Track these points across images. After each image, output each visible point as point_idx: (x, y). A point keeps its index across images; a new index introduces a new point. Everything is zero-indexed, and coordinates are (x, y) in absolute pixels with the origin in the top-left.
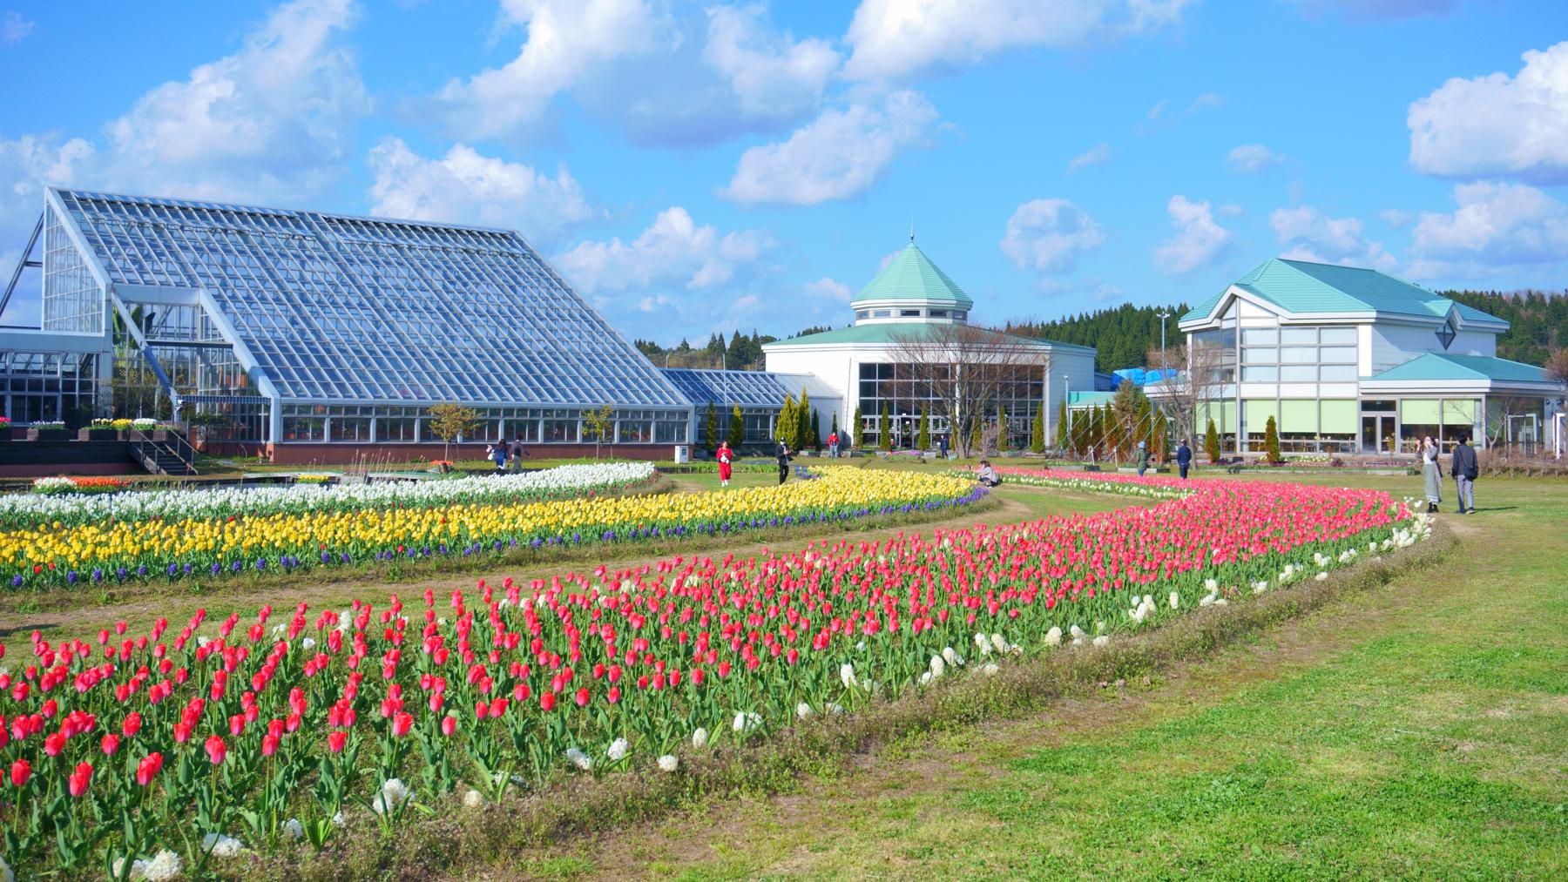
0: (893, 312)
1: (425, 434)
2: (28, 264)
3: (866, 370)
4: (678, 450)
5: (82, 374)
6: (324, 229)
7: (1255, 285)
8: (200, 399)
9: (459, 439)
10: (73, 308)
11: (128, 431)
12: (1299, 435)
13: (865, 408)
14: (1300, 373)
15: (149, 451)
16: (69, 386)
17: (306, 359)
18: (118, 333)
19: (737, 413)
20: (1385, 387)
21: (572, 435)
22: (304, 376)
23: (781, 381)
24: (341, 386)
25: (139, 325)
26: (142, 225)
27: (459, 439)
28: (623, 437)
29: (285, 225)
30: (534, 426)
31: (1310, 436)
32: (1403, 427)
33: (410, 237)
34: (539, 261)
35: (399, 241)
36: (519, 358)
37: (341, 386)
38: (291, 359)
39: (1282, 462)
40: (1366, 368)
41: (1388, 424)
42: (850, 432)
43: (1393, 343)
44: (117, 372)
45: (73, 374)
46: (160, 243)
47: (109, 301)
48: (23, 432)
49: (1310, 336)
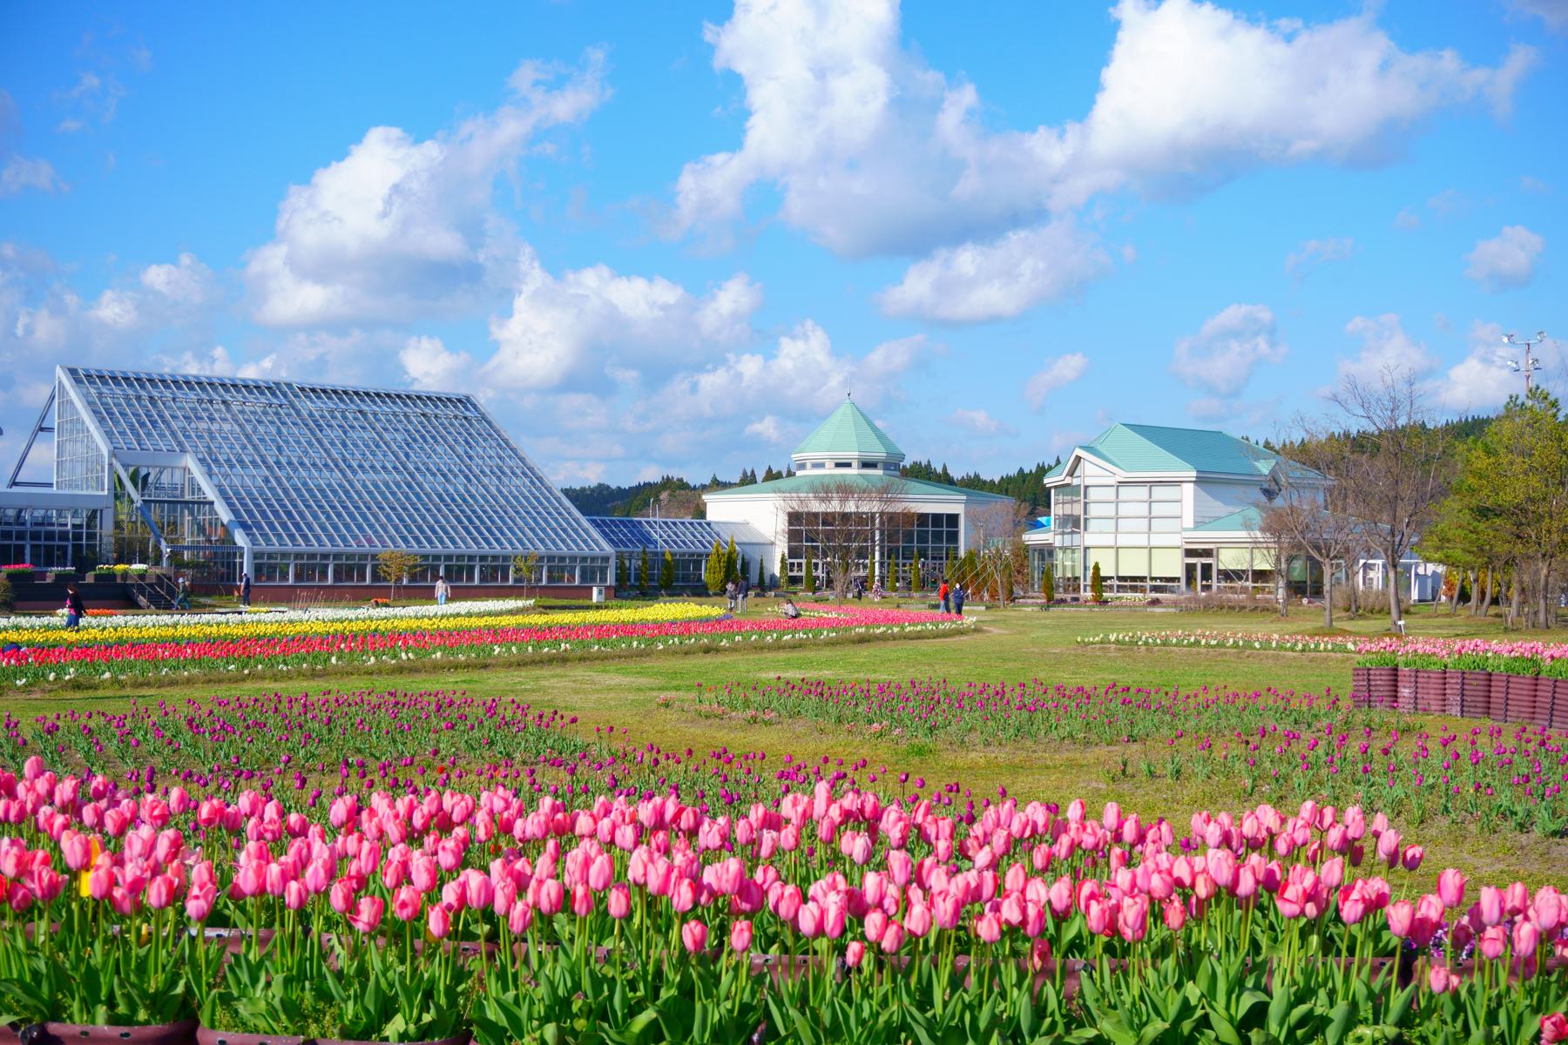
0: (830, 464)
1: (375, 577)
2: (42, 429)
3: (794, 518)
4: (595, 591)
5: (88, 526)
6: (296, 396)
7: (1099, 448)
8: (188, 548)
9: (405, 582)
10: (80, 470)
11: (125, 575)
12: (1134, 579)
13: (793, 553)
14: (1138, 523)
15: (141, 590)
16: (78, 537)
17: (275, 513)
18: (118, 493)
19: (668, 557)
20: (1204, 538)
21: (505, 578)
22: (272, 528)
23: (716, 528)
24: (304, 537)
25: (136, 485)
26: (139, 398)
27: (405, 582)
28: (550, 579)
29: (262, 393)
30: (471, 569)
31: (1142, 579)
32: (1219, 572)
33: (375, 403)
34: (489, 423)
35: (364, 407)
36: (463, 511)
37: (304, 537)
38: (263, 513)
39: (1106, 602)
40: (1189, 521)
41: (1207, 569)
42: (777, 573)
43: (1216, 498)
44: (118, 525)
45: (81, 526)
46: (154, 413)
47: (111, 465)
48: (43, 575)
49: (1142, 492)
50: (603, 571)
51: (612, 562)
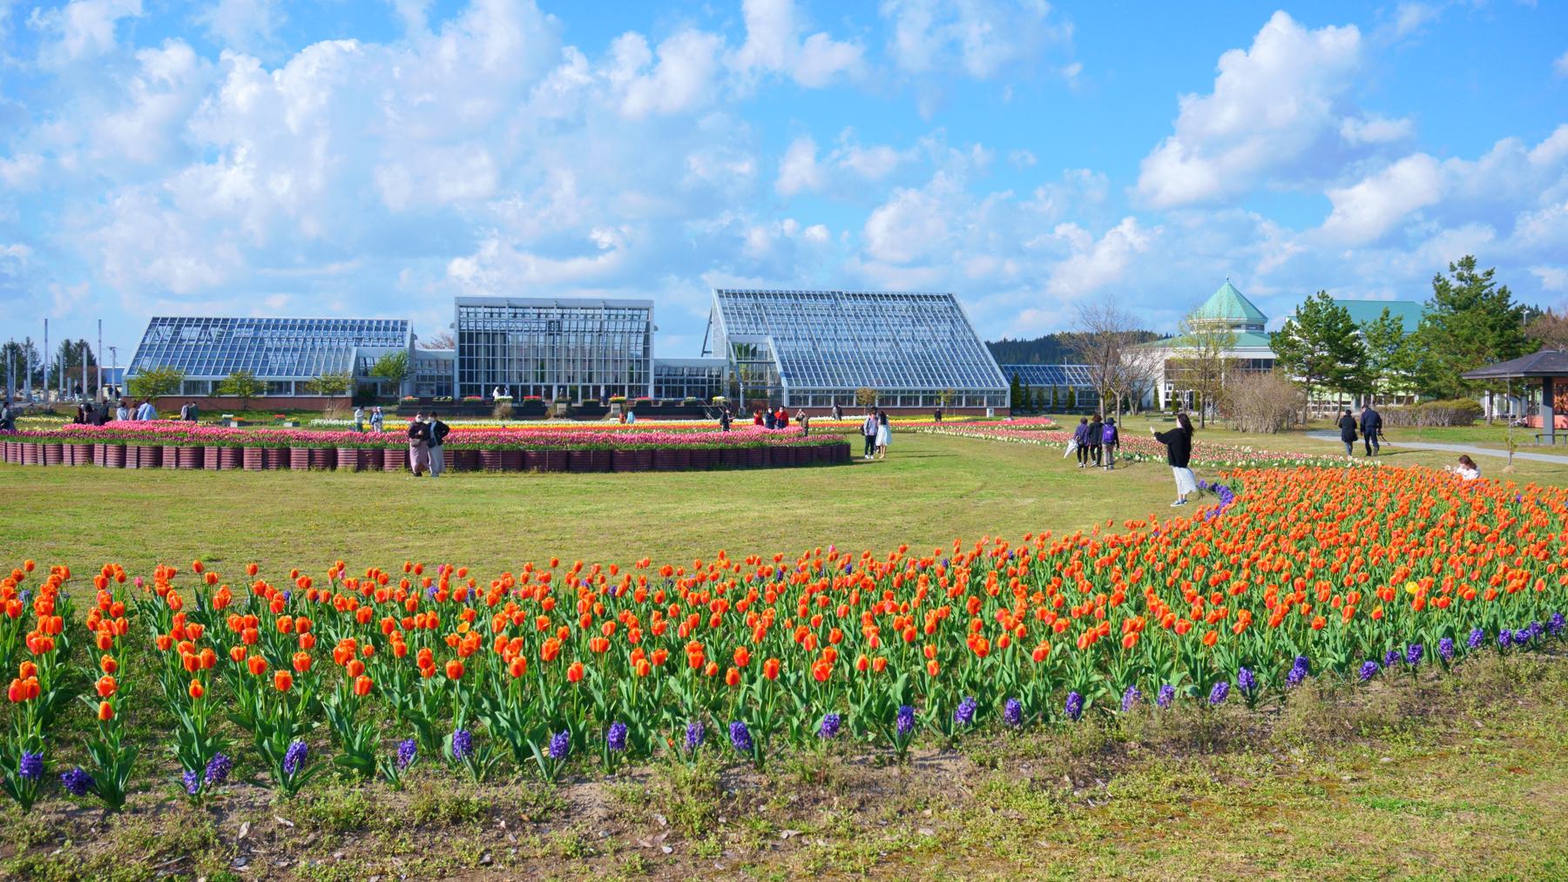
51: (1009, 394)
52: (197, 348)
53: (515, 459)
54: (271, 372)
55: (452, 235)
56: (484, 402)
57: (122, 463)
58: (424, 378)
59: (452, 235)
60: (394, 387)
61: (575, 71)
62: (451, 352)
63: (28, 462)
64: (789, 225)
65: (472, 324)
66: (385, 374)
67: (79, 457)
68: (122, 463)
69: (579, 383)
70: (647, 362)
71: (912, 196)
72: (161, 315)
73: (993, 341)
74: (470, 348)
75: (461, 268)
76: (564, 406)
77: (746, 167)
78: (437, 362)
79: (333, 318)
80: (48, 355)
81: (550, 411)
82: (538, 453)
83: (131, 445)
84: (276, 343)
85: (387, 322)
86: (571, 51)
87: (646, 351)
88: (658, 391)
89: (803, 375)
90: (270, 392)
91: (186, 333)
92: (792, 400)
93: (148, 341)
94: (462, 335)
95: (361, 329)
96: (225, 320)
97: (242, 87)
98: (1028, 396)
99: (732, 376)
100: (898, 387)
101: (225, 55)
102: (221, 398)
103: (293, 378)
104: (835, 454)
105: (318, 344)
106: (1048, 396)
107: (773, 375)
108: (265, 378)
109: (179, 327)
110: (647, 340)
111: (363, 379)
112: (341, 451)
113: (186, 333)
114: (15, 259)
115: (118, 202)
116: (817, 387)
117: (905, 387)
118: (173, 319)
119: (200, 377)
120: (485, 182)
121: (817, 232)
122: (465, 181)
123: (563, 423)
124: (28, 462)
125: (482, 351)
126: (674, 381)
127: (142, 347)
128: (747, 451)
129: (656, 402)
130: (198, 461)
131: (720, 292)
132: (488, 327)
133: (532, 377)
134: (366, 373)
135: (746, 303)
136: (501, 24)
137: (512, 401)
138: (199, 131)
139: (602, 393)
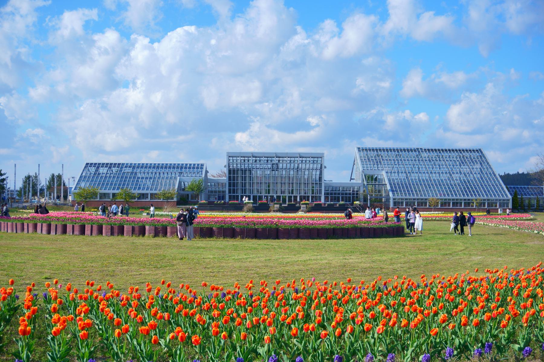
16: (353, 194)
21: (426, 205)
48: (336, 204)
50: (508, 204)
51: (511, 201)
52: (106, 177)
53: (230, 232)
54: (139, 188)
55: (238, 121)
56: (239, 204)
57: (49, 232)
58: (212, 192)
59: (238, 121)
60: (197, 196)
61: (300, 38)
62: (225, 179)
63: (9, 231)
64: (407, 114)
65: (235, 165)
66: (193, 190)
67: (31, 229)
68: (49, 232)
69: (287, 195)
70: (320, 184)
71: (474, 97)
72: (90, 162)
73: (503, 174)
74: (234, 177)
75: (241, 137)
76: (278, 206)
77: (386, 84)
78: (217, 183)
79: (181, 163)
80: (43, 181)
81: (271, 208)
82: (241, 229)
83: (53, 224)
84: (146, 175)
85: (194, 165)
86: (299, 28)
87: (320, 178)
88: (326, 198)
89: (400, 191)
90: (139, 198)
91: (101, 170)
92: (395, 203)
93: (84, 174)
94: (230, 171)
95: (182, 168)
96: (119, 164)
97: (140, 52)
98: (522, 202)
99: (364, 191)
100: (451, 197)
101: (133, 37)
102: (114, 201)
103: (149, 192)
104: (396, 232)
105: (162, 175)
106: (534, 202)
107: (386, 191)
108: (137, 192)
109: (98, 167)
110: (321, 174)
111: (182, 192)
112: (147, 227)
113: (101, 170)
114: (36, 136)
115: (82, 109)
116: (408, 197)
117: (455, 197)
118: (95, 164)
119: (107, 191)
120: (255, 95)
121: (422, 116)
122: (243, 95)
123: (250, 214)
124: (9, 231)
125: (240, 179)
126: (335, 194)
127: (81, 177)
128: (348, 229)
129: (325, 204)
130: (82, 231)
131: (359, 148)
132: (243, 167)
133: (263, 192)
134: (184, 190)
135: (373, 154)
136: (266, 15)
137: (253, 203)
138: (120, 72)
139: (298, 200)
